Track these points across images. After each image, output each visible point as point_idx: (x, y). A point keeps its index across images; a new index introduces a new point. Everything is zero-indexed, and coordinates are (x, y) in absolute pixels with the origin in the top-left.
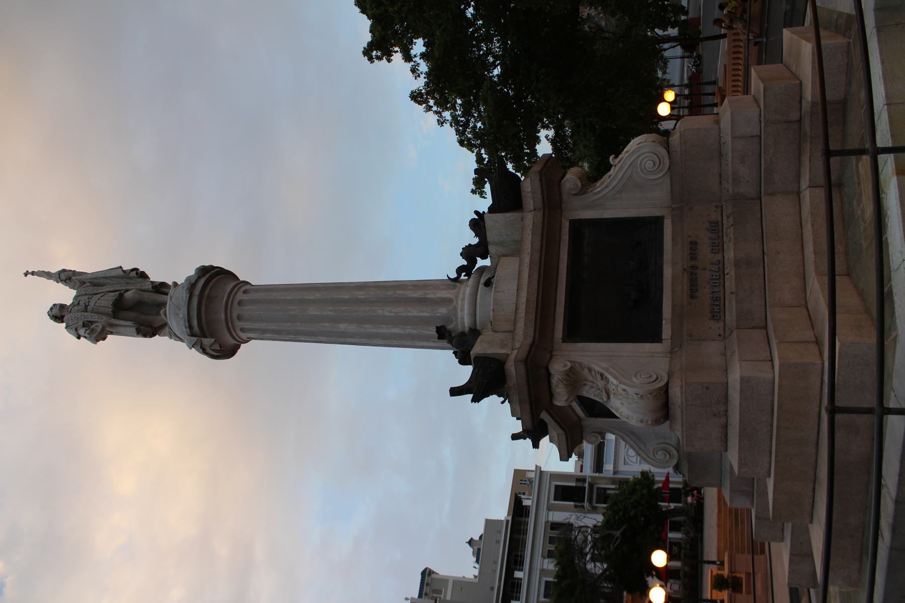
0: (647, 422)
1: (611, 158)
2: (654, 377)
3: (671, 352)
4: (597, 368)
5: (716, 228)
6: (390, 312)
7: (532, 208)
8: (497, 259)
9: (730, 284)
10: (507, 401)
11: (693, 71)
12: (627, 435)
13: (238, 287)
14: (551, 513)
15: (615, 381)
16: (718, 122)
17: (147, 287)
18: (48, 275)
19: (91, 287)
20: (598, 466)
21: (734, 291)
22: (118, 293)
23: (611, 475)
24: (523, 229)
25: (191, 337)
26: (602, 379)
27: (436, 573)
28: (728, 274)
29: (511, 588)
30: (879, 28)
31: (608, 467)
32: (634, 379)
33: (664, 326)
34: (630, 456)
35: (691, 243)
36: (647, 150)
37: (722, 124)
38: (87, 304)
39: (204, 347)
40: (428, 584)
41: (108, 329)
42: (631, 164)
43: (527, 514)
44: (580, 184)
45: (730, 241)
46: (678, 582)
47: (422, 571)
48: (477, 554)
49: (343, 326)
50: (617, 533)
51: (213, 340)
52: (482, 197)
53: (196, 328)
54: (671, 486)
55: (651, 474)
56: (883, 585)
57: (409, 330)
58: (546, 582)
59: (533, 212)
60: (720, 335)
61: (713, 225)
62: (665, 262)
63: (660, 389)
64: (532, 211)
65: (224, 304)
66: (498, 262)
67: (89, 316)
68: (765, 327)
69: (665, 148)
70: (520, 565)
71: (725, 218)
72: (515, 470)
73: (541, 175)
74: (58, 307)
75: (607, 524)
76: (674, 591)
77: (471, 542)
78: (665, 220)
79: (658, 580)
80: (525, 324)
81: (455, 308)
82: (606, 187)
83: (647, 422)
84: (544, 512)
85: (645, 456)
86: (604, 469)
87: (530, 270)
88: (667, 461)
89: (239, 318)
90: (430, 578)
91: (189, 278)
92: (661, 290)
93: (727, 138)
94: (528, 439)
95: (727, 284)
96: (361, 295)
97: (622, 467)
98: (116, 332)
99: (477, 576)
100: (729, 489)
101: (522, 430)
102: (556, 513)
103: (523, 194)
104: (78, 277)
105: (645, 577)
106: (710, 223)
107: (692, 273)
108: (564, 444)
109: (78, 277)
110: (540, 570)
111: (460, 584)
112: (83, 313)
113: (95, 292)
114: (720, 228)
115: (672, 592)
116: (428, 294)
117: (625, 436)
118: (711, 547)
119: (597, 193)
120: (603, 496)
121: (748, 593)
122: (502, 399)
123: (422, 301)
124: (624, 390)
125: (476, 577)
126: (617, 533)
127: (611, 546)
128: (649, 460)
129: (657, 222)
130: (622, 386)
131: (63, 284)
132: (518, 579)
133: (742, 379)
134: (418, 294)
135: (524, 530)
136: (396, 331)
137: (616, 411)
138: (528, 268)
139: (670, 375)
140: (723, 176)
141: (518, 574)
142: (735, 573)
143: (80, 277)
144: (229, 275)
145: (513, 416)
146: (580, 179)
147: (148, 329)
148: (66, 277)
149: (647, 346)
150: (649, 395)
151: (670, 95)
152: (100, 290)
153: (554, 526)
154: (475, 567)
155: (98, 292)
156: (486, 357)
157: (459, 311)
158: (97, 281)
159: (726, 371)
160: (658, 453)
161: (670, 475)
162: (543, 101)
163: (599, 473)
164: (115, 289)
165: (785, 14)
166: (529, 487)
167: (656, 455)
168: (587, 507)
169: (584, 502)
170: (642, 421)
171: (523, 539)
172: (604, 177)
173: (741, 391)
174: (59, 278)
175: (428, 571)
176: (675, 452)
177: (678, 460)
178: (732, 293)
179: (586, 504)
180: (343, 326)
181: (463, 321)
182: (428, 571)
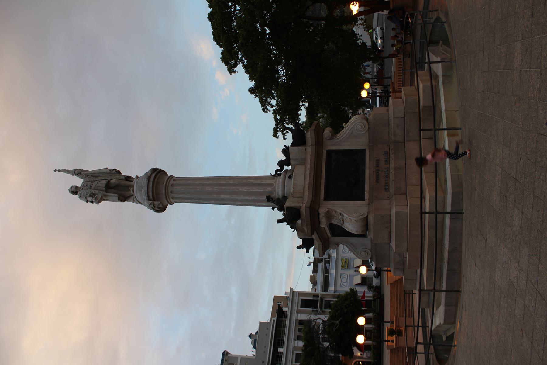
0: (359, 232)
1: (344, 124)
2: (362, 214)
3: (369, 205)
4: (338, 211)
5: (387, 154)
6: (245, 189)
7: (310, 145)
8: (294, 167)
9: (392, 177)
10: (296, 230)
11: (379, 68)
12: (349, 245)
13: (170, 178)
14: (299, 315)
15: (346, 216)
16: (388, 111)
17: (122, 178)
18: (68, 172)
19: (92, 178)
20: (325, 287)
21: (394, 179)
22: (107, 180)
23: (332, 293)
24: (306, 153)
25: (148, 201)
26: (341, 215)
27: (230, 354)
28: (391, 173)
29: (276, 357)
30: (444, 83)
31: (331, 289)
32: (354, 215)
33: (366, 195)
34: (344, 283)
35: (377, 160)
36: (359, 122)
37: (390, 112)
38: (91, 186)
39: (154, 205)
40: (226, 360)
41: (104, 198)
42: (352, 127)
43: (285, 317)
44: (331, 135)
45: (392, 159)
46: (370, 352)
47: (222, 352)
48: (254, 344)
49: (222, 196)
50: (337, 322)
51: (160, 202)
52: (276, 138)
53: (151, 197)
54: (366, 298)
55: (355, 290)
56: (446, 285)
57: (254, 197)
58: (297, 354)
59: (310, 147)
60: (388, 197)
61: (386, 153)
62: (366, 168)
63: (365, 218)
64: (310, 146)
65: (164, 186)
66: (295, 167)
67: (93, 192)
68: (406, 194)
69: (366, 121)
70: (281, 345)
71: (390, 150)
72: (274, 296)
73: (315, 131)
74: (75, 187)
75: (332, 318)
76: (368, 357)
77: (251, 336)
78: (366, 151)
79: (359, 351)
80: (308, 193)
81: (275, 188)
82: (342, 136)
83: (359, 232)
84: (295, 314)
85: (357, 254)
86: (329, 290)
87: (310, 171)
88: (366, 257)
89: (172, 192)
90: (227, 357)
91: (146, 174)
92: (365, 179)
93: (391, 118)
94: (304, 248)
95: (391, 177)
96: (231, 182)
97: (339, 289)
98: (106, 199)
99: (254, 355)
100: (393, 267)
101: (302, 244)
102: (302, 315)
103: (306, 139)
104: (85, 173)
105: (352, 347)
106: (385, 152)
107: (377, 173)
108: (321, 249)
109: (85, 173)
110: (293, 347)
111: (245, 360)
112: (89, 190)
113: (94, 180)
114: (389, 154)
115: (367, 357)
116: (262, 182)
117: (348, 245)
118: (388, 315)
119: (338, 139)
120: (328, 305)
121: (404, 336)
122: (293, 230)
123: (259, 185)
124: (350, 219)
125: (254, 355)
126: (337, 322)
127: (334, 329)
128: (358, 256)
129: (363, 152)
130: (349, 217)
131: (76, 176)
132: (281, 352)
133: (396, 212)
134: (258, 182)
135: (283, 325)
136: (247, 198)
137: (347, 228)
138: (309, 170)
139: (368, 213)
140: (390, 133)
141: (280, 350)
142: (399, 327)
143: (86, 173)
144: (163, 172)
145: (298, 237)
146: (331, 133)
147: (123, 198)
148: (78, 173)
149: (359, 203)
150: (360, 221)
151: (367, 86)
152: (97, 179)
153: (301, 322)
154: (252, 351)
155: (96, 180)
156: (291, 207)
157: (277, 189)
158: (95, 175)
159: (390, 210)
160: (363, 253)
161: (365, 293)
162: (309, 93)
163: (326, 292)
164: (105, 178)
165: (419, 58)
166: (286, 300)
167: (361, 254)
168: (319, 311)
169: (318, 308)
170: (357, 232)
171: (283, 331)
172: (341, 132)
173: (396, 217)
174: (74, 173)
175: (226, 353)
176: (370, 252)
177: (372, 256)
178: (393, 180)
179: (319, 310)
180: (222, 196)
181: (279, 193)
182: (226, 353)
